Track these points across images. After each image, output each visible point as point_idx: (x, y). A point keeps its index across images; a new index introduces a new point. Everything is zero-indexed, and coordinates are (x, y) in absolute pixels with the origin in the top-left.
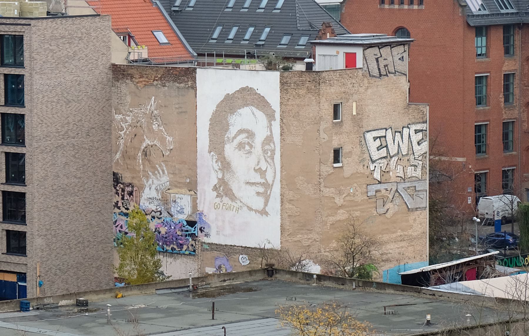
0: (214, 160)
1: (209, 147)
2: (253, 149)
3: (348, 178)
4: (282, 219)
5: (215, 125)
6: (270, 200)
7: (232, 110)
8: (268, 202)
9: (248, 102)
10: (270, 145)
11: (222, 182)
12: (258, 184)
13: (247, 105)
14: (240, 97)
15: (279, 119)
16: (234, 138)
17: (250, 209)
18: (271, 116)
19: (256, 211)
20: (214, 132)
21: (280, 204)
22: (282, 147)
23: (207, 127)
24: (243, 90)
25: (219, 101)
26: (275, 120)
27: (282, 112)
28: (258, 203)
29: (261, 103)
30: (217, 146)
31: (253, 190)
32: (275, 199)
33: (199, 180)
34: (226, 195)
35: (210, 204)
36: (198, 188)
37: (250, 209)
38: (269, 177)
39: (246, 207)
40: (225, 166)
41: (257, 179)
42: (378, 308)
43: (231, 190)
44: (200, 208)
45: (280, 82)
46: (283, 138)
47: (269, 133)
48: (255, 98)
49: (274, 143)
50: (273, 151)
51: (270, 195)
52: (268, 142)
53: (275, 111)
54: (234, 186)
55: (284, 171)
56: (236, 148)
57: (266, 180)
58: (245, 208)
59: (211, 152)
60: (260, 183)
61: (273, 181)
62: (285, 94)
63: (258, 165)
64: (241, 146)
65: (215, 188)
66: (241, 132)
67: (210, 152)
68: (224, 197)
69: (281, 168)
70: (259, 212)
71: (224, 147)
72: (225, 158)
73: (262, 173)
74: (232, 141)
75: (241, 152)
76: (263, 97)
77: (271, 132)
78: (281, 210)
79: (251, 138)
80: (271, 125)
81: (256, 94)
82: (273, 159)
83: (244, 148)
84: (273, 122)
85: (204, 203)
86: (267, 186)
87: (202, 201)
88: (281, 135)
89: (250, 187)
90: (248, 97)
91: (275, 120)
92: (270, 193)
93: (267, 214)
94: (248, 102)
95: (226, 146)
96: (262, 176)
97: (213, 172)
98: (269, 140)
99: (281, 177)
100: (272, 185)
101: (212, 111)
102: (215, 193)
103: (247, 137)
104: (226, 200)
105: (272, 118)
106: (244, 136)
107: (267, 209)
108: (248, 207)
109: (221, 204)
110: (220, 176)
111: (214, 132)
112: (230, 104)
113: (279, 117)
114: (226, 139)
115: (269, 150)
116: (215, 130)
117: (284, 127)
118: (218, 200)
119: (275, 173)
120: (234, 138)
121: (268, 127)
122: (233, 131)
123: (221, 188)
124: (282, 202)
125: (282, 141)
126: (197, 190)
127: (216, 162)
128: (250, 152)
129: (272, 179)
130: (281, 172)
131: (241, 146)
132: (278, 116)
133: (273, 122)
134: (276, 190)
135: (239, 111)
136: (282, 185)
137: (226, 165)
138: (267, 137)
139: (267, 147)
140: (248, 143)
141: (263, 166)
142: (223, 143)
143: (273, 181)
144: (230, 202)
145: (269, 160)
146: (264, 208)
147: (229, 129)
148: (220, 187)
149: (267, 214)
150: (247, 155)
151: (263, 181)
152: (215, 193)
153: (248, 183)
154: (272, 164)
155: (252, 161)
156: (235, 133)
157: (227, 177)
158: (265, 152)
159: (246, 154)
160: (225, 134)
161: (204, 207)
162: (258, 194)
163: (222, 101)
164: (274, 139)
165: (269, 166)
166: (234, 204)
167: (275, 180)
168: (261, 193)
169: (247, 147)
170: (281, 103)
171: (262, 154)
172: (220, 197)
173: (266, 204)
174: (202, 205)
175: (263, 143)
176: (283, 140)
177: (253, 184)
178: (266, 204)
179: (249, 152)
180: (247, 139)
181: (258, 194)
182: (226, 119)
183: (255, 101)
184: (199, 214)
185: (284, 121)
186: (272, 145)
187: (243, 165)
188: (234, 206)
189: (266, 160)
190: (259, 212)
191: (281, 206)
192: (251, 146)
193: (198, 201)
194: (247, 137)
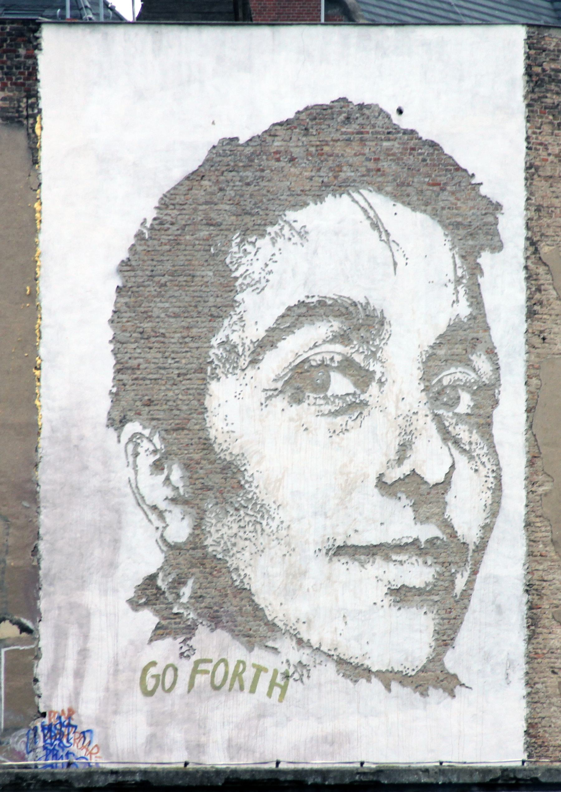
0: (145, 461)
1: (116, 397)
2: (374, 388)
3: (442, 483)
4: (533, 698)
5: (152, 289)
6: (469, 617)
7: (257, 218)
8: (455, 629)
9: (347, 173)
10: (468, 363)
11: (193, 559)
12: (400, 547)
13: (341, 187)
14: (297, 152)
15: (522, 243)
16: (268, 342)
17: (354, 670)
18: (472, 229)
19: (388, 678)
20: (147, 325)
21: (524, 633)
22: (533, 372)
23: (105, 301)
24: (315, 118)
25: (178, 174)
26: (497, 247)
27: (537, 210)
28: (409, 637)
29: (423, 173)
30: (160, 382)
31: (369, 581)
32: (499, 609)
33: (48, 562)
34: (215, 621)
35: (116, 672)
36: (42, 605)
37: (354, 670)
38: (465, 511)
39: (331, 667)
40: (213, 479)
41: (401, 523)
42: (217, 468)
43: (244, 592)
44: (55, 699)
45: (529, 72)
46: (538, 326)
47: (464, 309)
48: (388, 153)
49: (491, 353)
50: (487, 394)
51: (467, 594)
52: (459, 349)
53: (498, 207)
54: (264, 577)
55: (541, 478)
56: (272, 394)
57: (447, 525)
58: (329, 671)
59: (123, 421)
60: (414, 547)
61: (487, 528)
62: (547, 128)
63: (400, 461)
64: (302, 381)
65: (149, 593)
66: (303, 313)
67: (117, 422)
68: (202, 632)
69: (531, 463)
70: (404, 679)
71: (202, 393)
72: (207, 445)
73: (428, 497)
74: (254, 362)
75: (306, 411)
76: (433, 145)
77: (476, 299)
78: (531, 658)
79: (364, 341)
80: (475, 270)
81: (393, 131)
82: (484, 425)
83: (324, 386)
84: (486, 259)
85: (79, 675)
86: (454, 555)
87: (70, 664)
88: (531, 314)
89: (354, 567)
90: (343, 146)
91: (497, 247)
92: (470, 583)
93: (449, 683)
94: (347, 173)
95: (213, 386)
96: (424, 509)
97: (135, 518)
98: (465, 338)
99: (531, 506)
100: (481, 547)
101: (135, 228)
102: (148, 619)
103: (342, 338)
104: (211, 642)
105: (482, 239)
106: (321, 330)
107: (451, 661)
108: (341, 662)
109: (185, 667)
110: (179, 529)
111: (147, 325)
112: (237, 187)
113: (523, 232)
114: (215, 352)
115: (467, 387)
116: (149, 318)
117: (544, 278)
118: (166, 650)
119: (497, 489)
120: (268, 342)
121: (458, 281)
122: (257, 312)
123: (186, 591)
124: (533, 622)
125: (537, 341)
126: (35, 614)
127: (157, 467)
128: (354, 407)
129: (480, 518)
130: (531, 483)
131: (302, 381)
132: (513, 226)
133: (486, 259)
134: (505, 565)
135: (291, 215)
136: (532, 542)
137: (217, 479)
138: (455, 327)
139: (452, 374)
140: (348, 366)
141: (431, 459)
142: (199, 376)
143: (487, 528)
144: (236, 652)
145: (463, 432)
146: (436, 659)
147: (233, 304)
148: (180, 582)
149: (449, 683)
150: (340, 420)
151: (428, 532)
152: (148, 619)
153: (341, 551)
154: (481, 450)
155: (368, 446)
156: (270, 323)
157: (221, 531)
158: (439, 397)
159: (336, 414)
160: (213, 331)
161: (77, 693)
162: (401, 595)
163: (195, 177)
164: (493, 332)
165: (462, 461)
166: (260, 657)
167: (500, 522)
168: (419, 592)
169: (340, 384)
170: (532, 170)
171: (424, 410)
172: (175, 634)
173: (445, 639)
174: (67, 682)
175: (431, 357)
176: (537, 339)
177: (373, 551)
178: (445, 639)
179: (351, 406)
180: (338, 348)
181: (401, 595)
182: (217, 259)
183: (384, 165)
184: (49, 728)
185: (545, 249)
186: (482, 363)
187: (309, 469)
188: (259, 670)
189: (447, 435)
190: (404, 679)
191: (530, 639)
192: (363, 377)
193: (42, 668)
194: (342, 338)
